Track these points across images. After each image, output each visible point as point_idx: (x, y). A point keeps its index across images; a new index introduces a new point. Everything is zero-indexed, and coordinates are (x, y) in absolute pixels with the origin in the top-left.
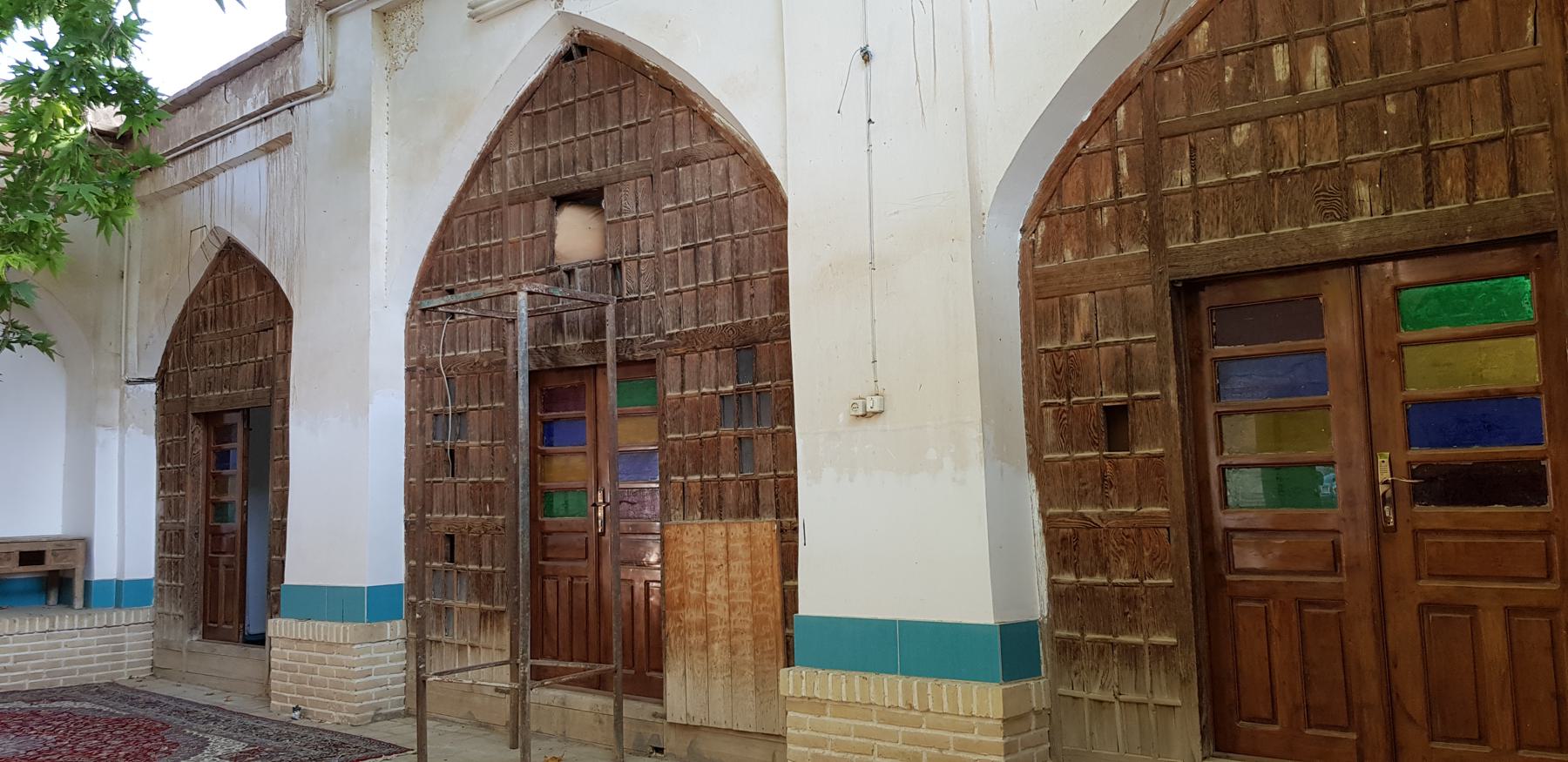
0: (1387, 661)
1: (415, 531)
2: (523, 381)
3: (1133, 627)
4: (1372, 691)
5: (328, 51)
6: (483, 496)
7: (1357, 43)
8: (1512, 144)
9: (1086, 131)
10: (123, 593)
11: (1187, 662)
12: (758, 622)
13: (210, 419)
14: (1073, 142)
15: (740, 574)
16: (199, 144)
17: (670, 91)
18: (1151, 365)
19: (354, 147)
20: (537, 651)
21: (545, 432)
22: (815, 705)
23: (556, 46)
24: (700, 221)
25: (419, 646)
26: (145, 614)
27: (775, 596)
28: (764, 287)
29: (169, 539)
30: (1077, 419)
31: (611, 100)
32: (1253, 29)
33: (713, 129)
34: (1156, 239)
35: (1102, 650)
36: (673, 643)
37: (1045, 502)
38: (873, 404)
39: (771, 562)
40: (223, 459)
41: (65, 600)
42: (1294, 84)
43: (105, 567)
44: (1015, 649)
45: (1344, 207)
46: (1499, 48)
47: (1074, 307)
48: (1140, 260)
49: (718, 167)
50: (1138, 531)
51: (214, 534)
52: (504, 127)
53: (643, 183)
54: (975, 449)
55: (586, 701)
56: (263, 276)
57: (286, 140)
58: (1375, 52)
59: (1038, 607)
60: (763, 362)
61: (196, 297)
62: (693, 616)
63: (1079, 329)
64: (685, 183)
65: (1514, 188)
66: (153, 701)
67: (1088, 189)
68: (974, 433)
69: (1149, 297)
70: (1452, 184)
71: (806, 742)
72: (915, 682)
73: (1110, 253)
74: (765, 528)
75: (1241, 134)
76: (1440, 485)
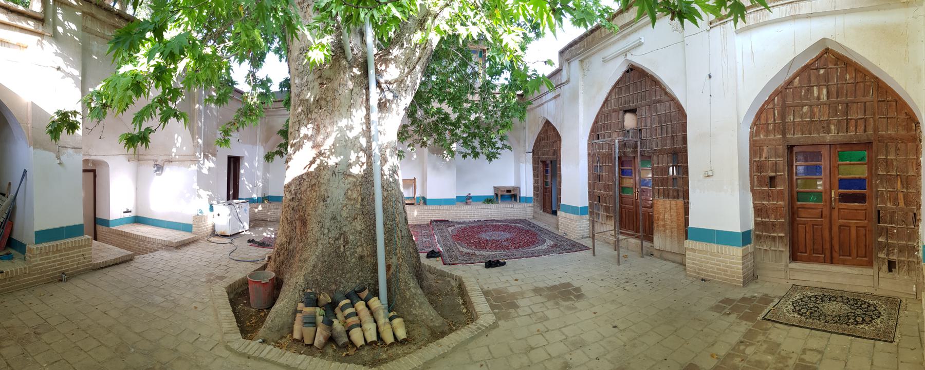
0: (831, 238)
1: (591, 195)
2: (617, 159)
3: (774, 231)
4: (827, 246)
5: (568, 72)
6: (607, 187)
7: (834, 89)
8: (866, 120)
9: (767, 102)
10: (527, 200)
11: (787, 240)
12: (678, 226)
13: (543, 162)
14: (763, 105)
15: (674, 213)
16: (540, 97)
17: (655, 82)
18: (781, 166)
19: (574, 97)
20: (621, 227)
21: (623, 172)
22: (694, 250)
23: (625, 68)
24: (663, 119)
25: (593, 223)
26: (531, 204)
27: (683, 220)
28: (680, 138)
29: (536, 189)
30: (762, 179)
31: (639, 84)
32: (810, 82)
33: (666, 93)
34: (784, 134)
35: (767, 237)
36: (656, 229)
37: (754, 200)
38: (710, 173)
39: (682, 211)
40: (547, 171)
41: (516, 200)
42: (819, 98)
43: (523, 194)
44: (746, 237)
45: (829, 132)
46: (864, 96)
47: (763, 150)
48: (780, 139)
49: (667, 104)
50: (776, 209)
51: (545, 188)
52: (611, 91)
53: (647, 108)
54: (737, 187)
55: (633, 241)
56: (554, 129)
57: (559, 95)
58: (837, 93)
59: (751, 226)
60: (680, 158)
61: (540, 133)
62: (661, 223)
63: (764, 156)
64: (659, 108)
65: (865, 131)
66: (534, 226)
67: (767, 119)
68: (737, 183)
69: (782, 149)
70: (852, 128)
71: (690, 259)
72: (720, 246)
73: (772, 137)
74: (680, 202)
75: (805, 109)
76: (844, 198)
